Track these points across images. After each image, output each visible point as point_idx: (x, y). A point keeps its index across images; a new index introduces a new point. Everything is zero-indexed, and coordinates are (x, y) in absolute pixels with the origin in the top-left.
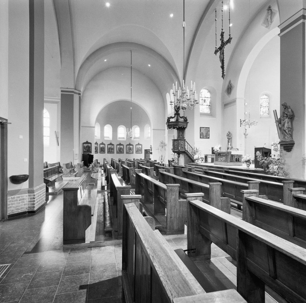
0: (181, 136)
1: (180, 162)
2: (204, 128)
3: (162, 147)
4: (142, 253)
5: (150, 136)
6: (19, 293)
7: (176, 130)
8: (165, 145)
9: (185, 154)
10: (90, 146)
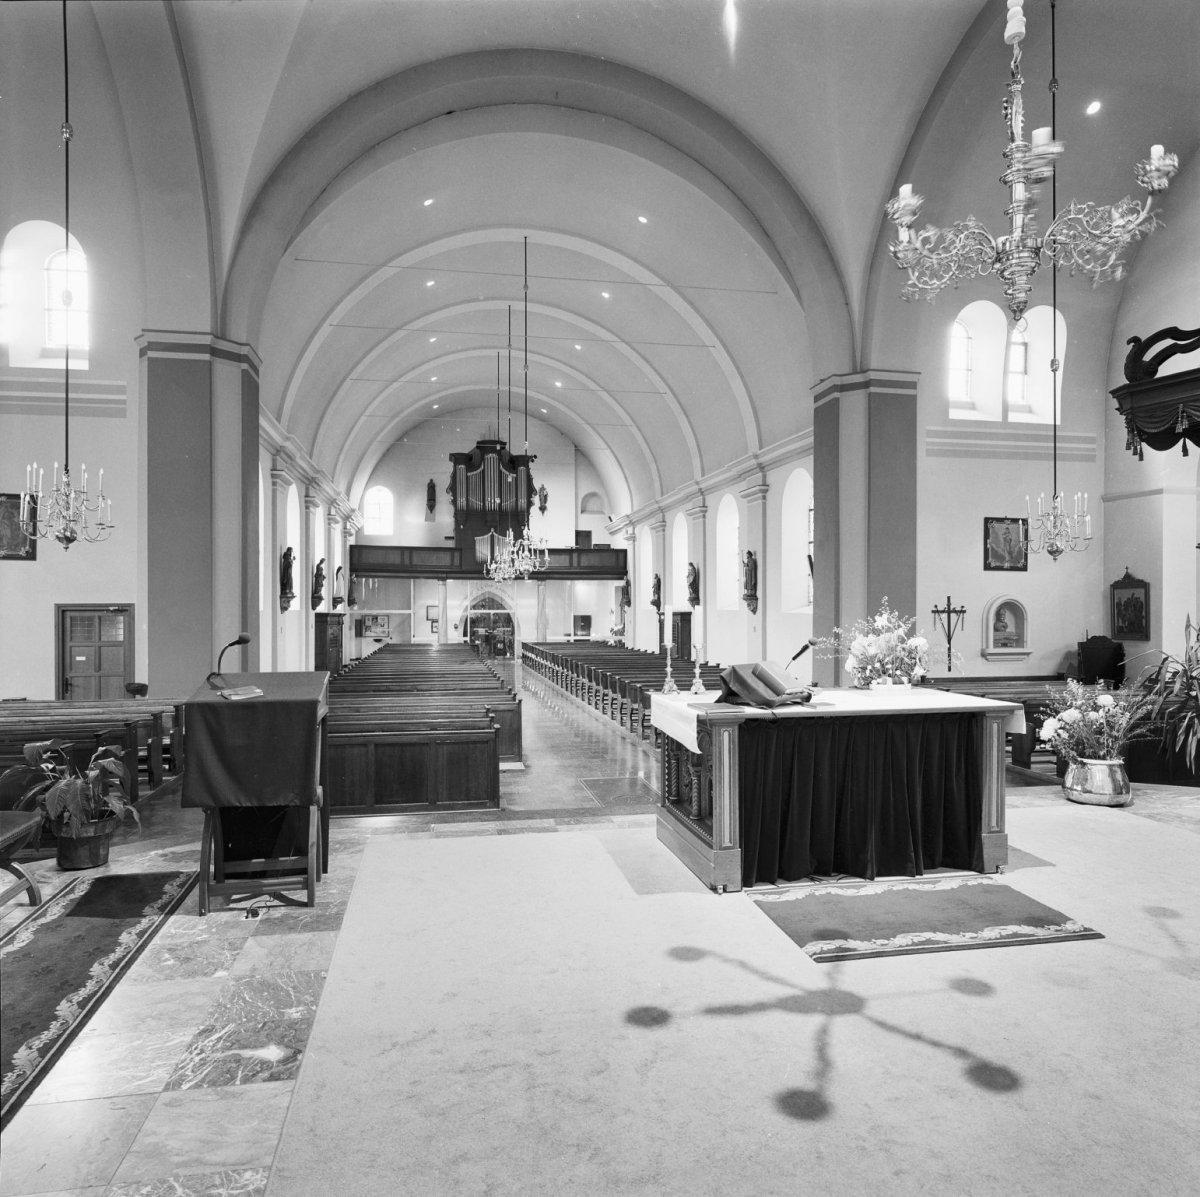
6: (217, 933)
10: (1142, 599)
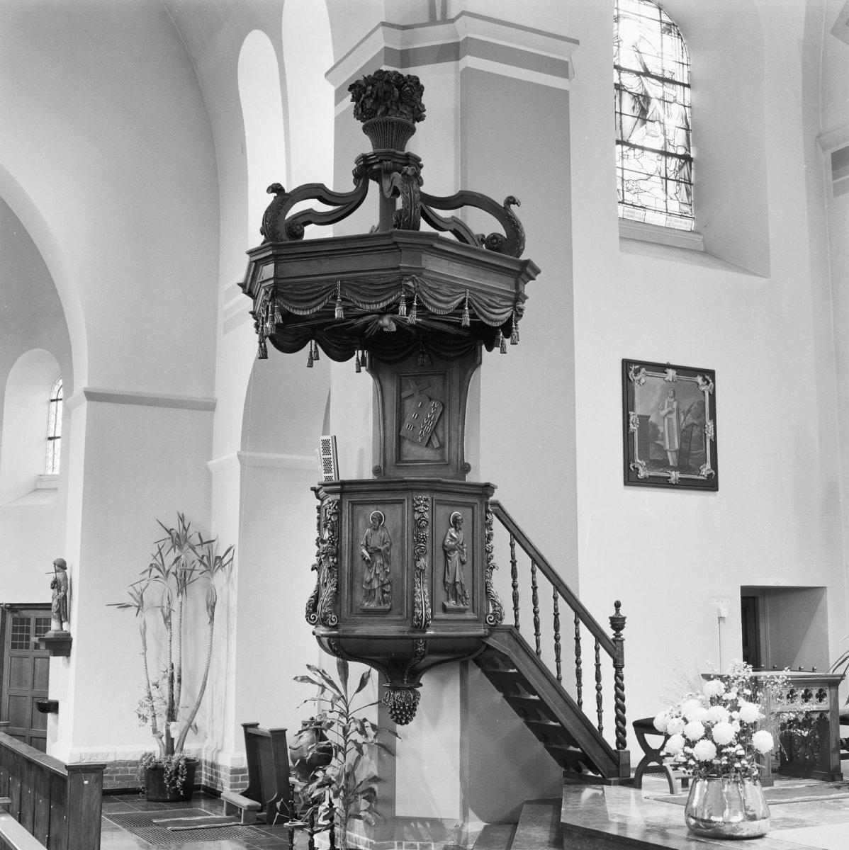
0: (427, 454)
1: (404, 766)
2: (661, 368)
3: (183, 585)
4: (170, 611)
5: (57, 472)
7: (366, 378)
8: (213, 563)
9: (476, 673)
